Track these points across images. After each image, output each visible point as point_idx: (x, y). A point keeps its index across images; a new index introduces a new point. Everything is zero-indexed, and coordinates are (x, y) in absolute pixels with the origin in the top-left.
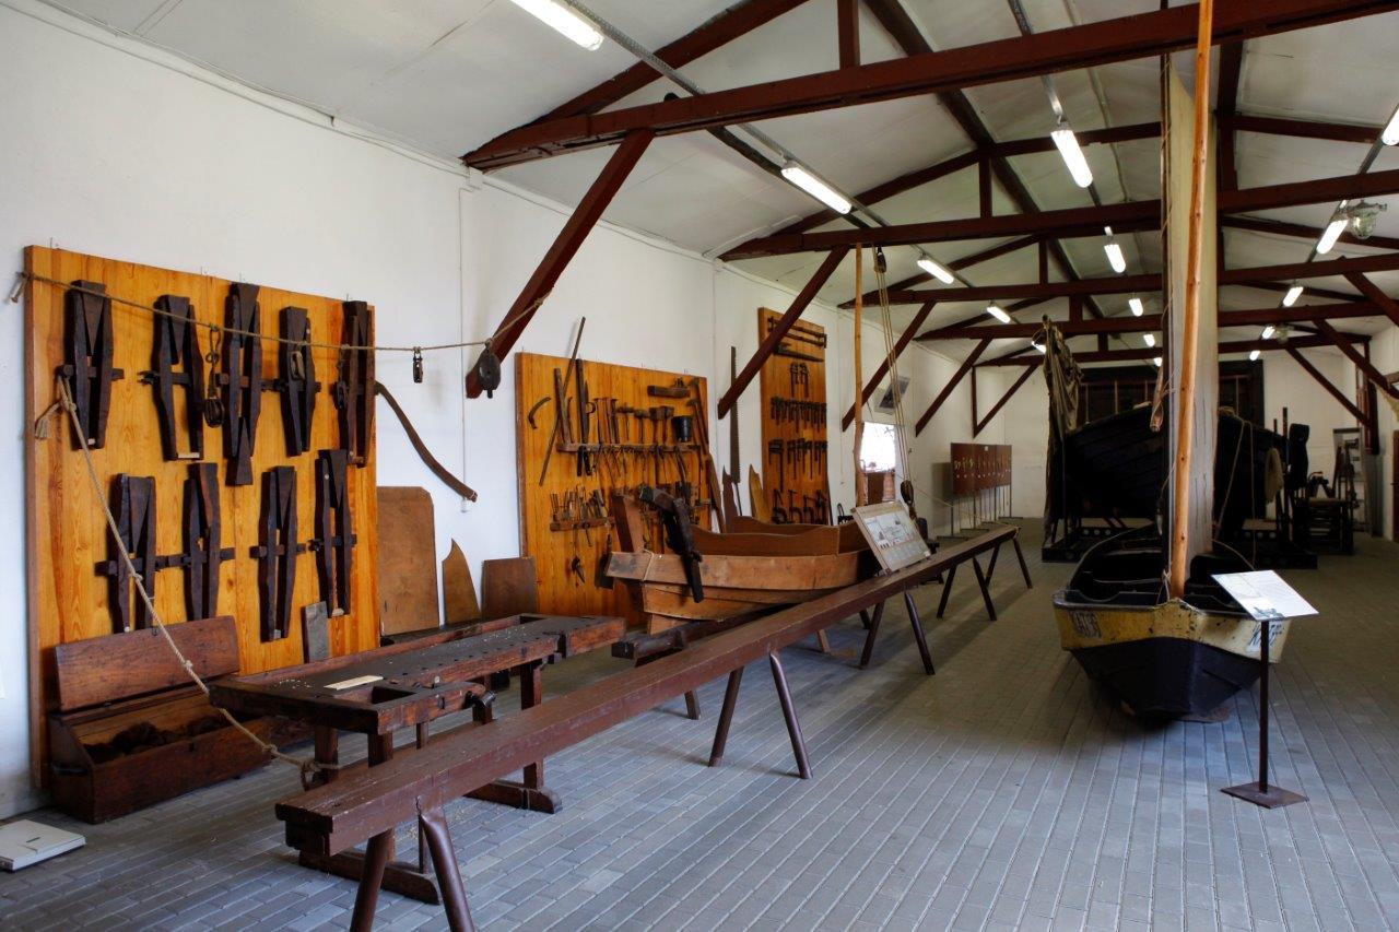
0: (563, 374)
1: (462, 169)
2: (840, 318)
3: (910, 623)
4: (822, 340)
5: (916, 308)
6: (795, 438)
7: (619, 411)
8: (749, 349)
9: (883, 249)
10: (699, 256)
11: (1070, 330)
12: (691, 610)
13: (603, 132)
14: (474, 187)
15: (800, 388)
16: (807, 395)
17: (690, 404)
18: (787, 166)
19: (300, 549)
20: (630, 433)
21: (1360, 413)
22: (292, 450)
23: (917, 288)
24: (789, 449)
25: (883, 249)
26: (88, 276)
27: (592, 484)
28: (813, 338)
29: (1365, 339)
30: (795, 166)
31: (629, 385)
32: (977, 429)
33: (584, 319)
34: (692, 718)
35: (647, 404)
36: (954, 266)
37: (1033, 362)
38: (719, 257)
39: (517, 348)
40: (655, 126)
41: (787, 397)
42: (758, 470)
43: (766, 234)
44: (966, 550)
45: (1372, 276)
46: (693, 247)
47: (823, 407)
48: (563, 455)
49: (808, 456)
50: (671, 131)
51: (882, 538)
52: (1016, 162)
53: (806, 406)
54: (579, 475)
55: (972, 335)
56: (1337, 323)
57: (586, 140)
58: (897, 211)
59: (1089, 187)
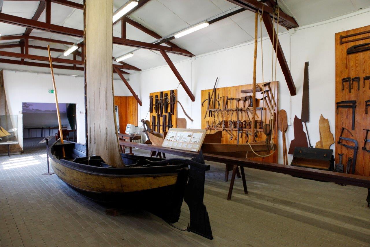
7: (229, 99)
20: (233, 105)
26: (236, 97)
44: (203, 237)
54: (209, 117)
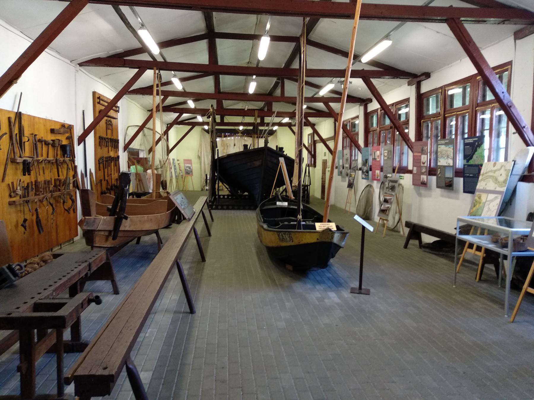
3: (195, 242)
10: (69, 62)
17: (67, 138)
18: (140, 28)
27: (26, 179)
31: (42, 128)
33: (21, 93)
34: (116, 294)
35: (50, 137)
37: (194, 125)
38: (78, 64)
41: (105, 136)
42: (93, 171)
46: (67, 58)
47: (118, 140)
48: (14, 164)
49: (112, 164)
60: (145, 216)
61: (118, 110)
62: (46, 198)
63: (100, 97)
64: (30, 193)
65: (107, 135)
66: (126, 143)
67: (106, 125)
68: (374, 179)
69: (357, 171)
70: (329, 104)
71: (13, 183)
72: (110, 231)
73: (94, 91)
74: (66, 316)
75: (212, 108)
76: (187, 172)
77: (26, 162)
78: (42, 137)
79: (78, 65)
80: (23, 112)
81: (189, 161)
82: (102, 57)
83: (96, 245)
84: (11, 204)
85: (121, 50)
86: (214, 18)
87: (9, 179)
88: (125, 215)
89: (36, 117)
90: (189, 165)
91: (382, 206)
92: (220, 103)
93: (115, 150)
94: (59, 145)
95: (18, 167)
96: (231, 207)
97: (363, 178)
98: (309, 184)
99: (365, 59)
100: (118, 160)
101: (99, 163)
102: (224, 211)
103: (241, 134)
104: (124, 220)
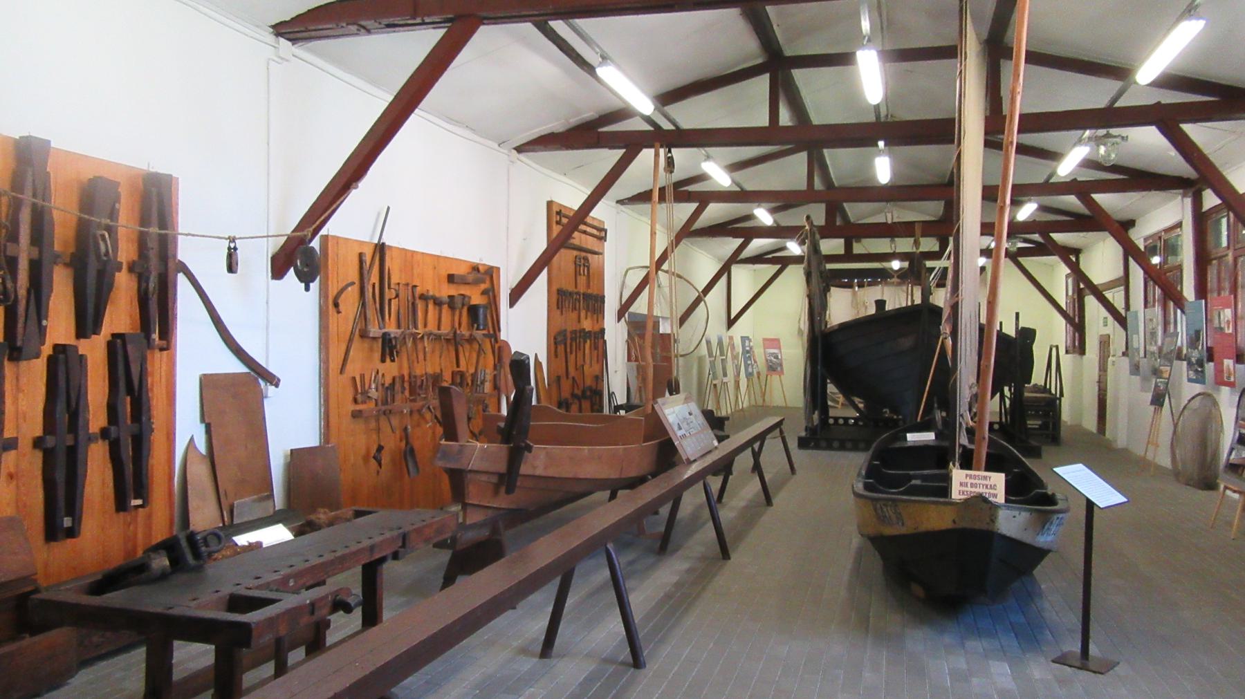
0: (368, 259)
1: (271, 38)
2: (618, 213)
4: (603, 234)
5: (693, 206)
6: (577, 327)
8: (540, 245)
9: (673, 150)
10: (496, 146)
11: (828, 231)
12: (503, 502)
13: (429, 15)
14: (282, 59)
15: (582, 280)
16: (588, 286)
17: (484, 293)
18: (601, 64)
19: (91, 439)
21: (1069, 315)
22: (81, 332)
23: (691, 188)
24: (571, 339)
25: (673, 150)
27: (390, 370)
28: (595, 232)
29: (1077, 252)
30: (610, 65)
32: (731, 322)
33: (388, 208)
35: (446, 291)
36: (735, 167)
37: (785, 262)
38: (515, 149)
39: (323, 232)
40: (485, 14)
41: (571, 288)
43: (561, 129)
45: (1097, 197)
50: (500, 21)
51: (680, 428)
52: (799, 75)
53: (587, 297)
55: (735, 234)
56: (1058, 237)
57: (410, 22)
58: (690, 115)
59: (875, 106)
60: (584, 449)
61: (604, 235)
62: (429, 408)
63: (561, 211)
64: (399, 397)
65: (576, 287)
66: (623, 303)
67: (573, 267)
68: (1220, 381)
69: (1176, 363)
70: (1092, 197)
71: (362, 376)
72: (501, 476)
73: (549, 199)
74: (253, 625)
75: (808, 224)
76: (771, 366)
77: (388, 337)
78: (428, 290)
79: (515, 152)
80: (387, 244)
81: (773, 342)
82: (558, 132)
83: (470, 502)
84: (356, 415)
85: (592, 113)
86: (775, 27)
87: (354, 369)
88: (528, 442)
89: (417, 252)
90: (775, 351)
91: (1234, 453)
92: (834, 209)
93: (595, 316)
94: (463, 305)
95: (375, 345)
96: (849, 445)
97: (1190, 380)
98: (1058, 396)
99: (1146, 73)
100: (603, 337)
101: (555, 343)
102: (833, 453)
103: (899, 280)
104: (526, 453)
